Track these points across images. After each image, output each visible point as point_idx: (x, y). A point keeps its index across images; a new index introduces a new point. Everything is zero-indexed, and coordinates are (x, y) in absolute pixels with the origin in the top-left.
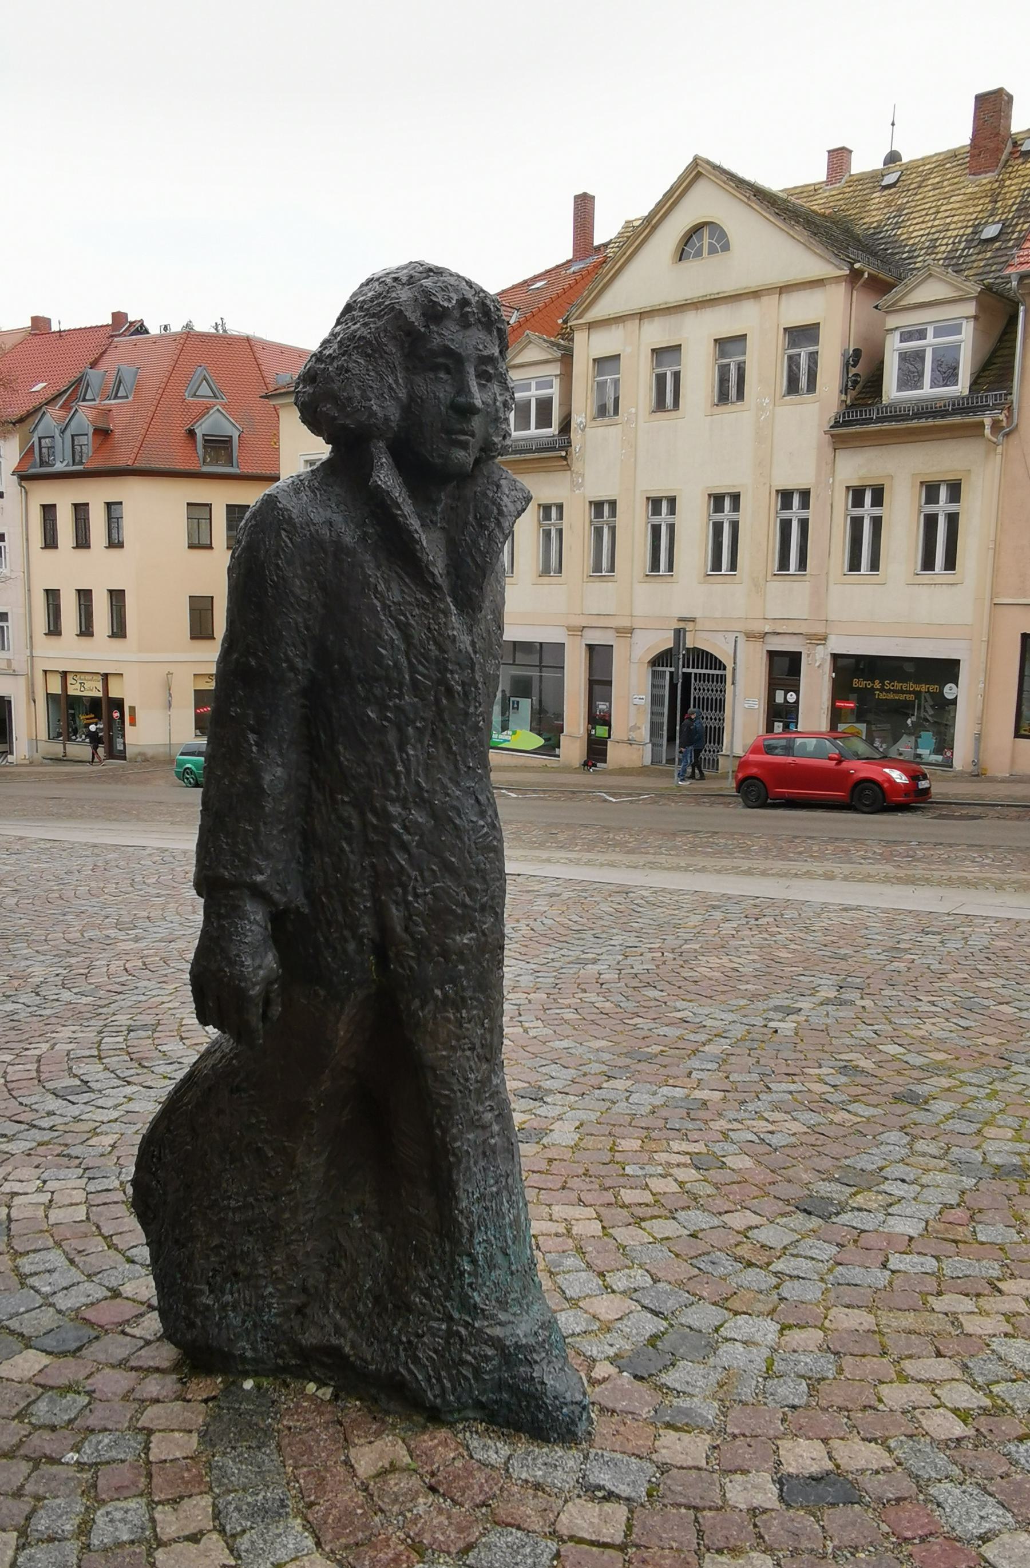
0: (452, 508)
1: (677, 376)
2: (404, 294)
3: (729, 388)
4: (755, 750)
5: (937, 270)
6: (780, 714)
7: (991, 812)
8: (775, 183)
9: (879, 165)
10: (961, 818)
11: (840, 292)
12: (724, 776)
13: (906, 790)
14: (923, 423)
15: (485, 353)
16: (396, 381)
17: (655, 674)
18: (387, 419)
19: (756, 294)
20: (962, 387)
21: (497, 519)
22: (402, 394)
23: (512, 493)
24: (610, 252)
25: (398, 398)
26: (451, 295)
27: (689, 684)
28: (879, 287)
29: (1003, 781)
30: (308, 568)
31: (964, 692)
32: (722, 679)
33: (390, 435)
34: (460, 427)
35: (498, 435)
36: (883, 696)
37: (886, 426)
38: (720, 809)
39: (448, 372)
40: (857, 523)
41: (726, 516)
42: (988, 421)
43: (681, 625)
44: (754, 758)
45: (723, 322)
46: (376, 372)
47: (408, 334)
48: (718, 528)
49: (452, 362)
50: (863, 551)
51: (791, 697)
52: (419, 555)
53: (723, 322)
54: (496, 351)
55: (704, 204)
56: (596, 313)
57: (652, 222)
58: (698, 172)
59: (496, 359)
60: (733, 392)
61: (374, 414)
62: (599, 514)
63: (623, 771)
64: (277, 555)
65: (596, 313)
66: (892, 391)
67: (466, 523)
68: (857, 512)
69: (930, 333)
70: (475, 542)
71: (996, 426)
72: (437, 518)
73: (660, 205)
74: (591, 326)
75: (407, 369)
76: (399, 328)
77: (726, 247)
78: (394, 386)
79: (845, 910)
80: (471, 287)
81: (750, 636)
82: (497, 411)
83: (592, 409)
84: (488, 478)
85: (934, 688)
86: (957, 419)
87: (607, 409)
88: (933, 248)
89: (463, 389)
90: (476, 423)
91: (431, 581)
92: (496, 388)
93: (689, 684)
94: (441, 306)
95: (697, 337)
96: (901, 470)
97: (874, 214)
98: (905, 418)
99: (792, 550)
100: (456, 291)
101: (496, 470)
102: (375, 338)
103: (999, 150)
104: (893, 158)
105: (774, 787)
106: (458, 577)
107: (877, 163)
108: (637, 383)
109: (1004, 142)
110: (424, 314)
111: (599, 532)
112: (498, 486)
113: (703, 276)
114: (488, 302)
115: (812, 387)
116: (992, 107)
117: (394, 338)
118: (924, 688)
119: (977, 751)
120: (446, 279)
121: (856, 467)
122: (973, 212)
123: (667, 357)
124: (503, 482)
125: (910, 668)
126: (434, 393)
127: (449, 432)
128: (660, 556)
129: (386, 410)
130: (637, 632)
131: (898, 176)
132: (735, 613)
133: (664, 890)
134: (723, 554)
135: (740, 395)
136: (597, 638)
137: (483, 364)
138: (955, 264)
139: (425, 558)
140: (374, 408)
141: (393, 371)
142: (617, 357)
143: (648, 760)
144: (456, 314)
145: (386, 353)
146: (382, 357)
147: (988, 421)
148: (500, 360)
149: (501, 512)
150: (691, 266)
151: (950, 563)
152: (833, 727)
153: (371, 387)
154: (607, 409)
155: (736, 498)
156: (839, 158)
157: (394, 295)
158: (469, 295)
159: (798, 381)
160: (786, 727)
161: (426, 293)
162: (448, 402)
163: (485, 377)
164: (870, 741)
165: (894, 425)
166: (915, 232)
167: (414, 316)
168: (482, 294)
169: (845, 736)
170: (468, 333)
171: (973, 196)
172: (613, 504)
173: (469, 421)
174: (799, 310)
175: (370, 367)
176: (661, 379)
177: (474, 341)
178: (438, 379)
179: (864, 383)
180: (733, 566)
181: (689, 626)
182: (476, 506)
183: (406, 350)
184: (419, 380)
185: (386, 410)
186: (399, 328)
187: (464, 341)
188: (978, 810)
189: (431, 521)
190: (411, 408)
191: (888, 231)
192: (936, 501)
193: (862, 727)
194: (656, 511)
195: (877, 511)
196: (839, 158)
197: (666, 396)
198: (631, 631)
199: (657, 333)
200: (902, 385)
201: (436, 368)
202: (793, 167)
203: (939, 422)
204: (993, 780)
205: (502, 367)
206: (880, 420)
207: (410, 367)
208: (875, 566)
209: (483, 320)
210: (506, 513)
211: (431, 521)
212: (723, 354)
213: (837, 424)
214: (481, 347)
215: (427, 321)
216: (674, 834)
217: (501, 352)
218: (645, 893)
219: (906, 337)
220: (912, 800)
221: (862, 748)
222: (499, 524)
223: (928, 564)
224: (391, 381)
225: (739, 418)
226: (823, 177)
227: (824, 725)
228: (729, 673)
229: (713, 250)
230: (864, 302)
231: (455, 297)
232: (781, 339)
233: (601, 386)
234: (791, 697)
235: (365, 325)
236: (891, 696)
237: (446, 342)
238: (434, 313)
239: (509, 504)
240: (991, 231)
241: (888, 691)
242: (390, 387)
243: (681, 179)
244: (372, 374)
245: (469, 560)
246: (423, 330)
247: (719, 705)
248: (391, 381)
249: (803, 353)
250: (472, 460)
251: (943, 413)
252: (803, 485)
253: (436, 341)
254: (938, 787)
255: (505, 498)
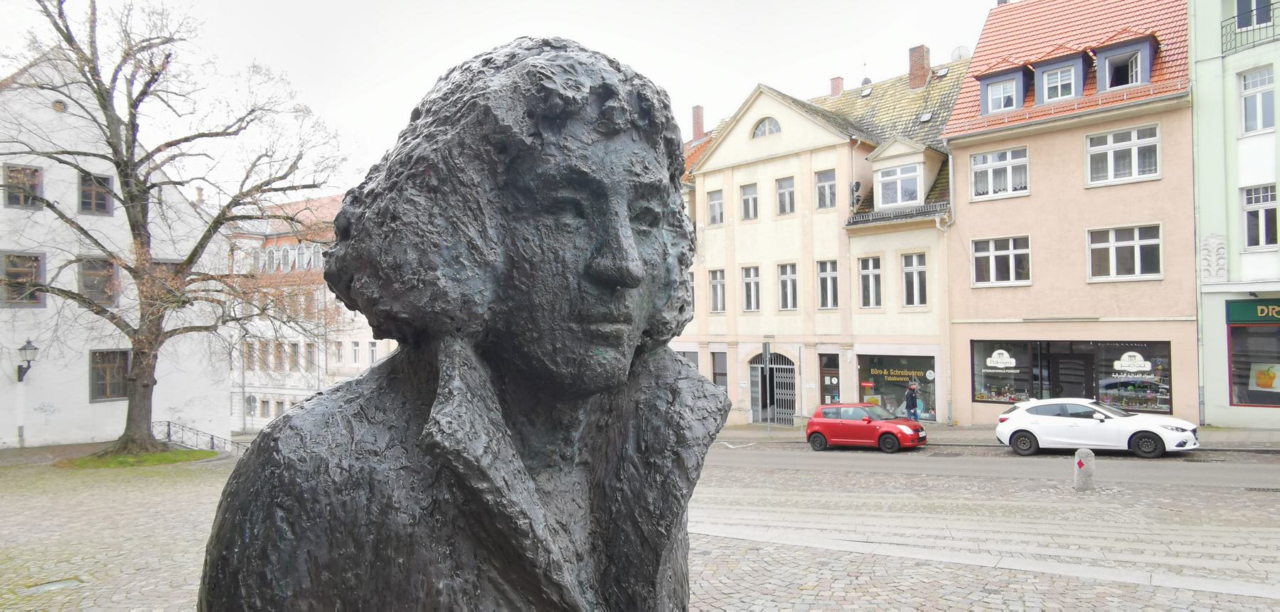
0: (599, 428)
1: (755, 200)
2: (497, 82)
3: (785, 206)
4: (817, 415)
5: (899, 138)
6: (829, 391)
7: (966, 450)
8: (803, 97)
9: (860, 86)
10: (949, 455)
11: (845, 151)
12: (798, 429)
13: (912, 438)
14: (899, 221)
15: (646, 179)
16: (483, 233)
17: (752, 369)
18: (466, 302)
19: (797, 154)
20: (920, 201)
21: (676, 453)
22: (496, 256)
23: (700, 403)
24: (713, 135)
25: (487, 264)
26: (582, 79)
27: (773, 379)
28: (868, 148)
29: (969, 429)
30: (325, 575)
31: (938, 375)
32: (792, 371)
33: (475, 327)
34: (603, 310)
35: (671, 308)
36: (890, 379)
37: (878, 223)
38: (798, 452)
39: (579, 212)
40: (865, 279)
41: (789, 276)
42: (937, 220)
43: (766, 340)
44: (816, 420)
45: (781, 170)
46: (447, 219)
47: (502, 148)
48: (784, 284)
49: (586, 195)
50: (870, 294)
51: (835, 381)
52: (529, 555)
53: (781, 170)
54: (665, 176)
55: (765, 107)
56: (707, 168)
57: (736, 119)
58: (759, 92)
59: (666, 189)
60: (788, 208)
61: (441, 295)
62: (714, 277)
63: (736, 427)
64: (264, 556)
65: (707, 168)
66: (879, 204)
67: (622, 458)
68: (865, 272)
69: (899, 171)
70: (639, 496)
71: (943, 222)
72: (573, 451)
73: (741, 109)
74: (705, 174)
75: (504, 211)
76: (485, 138)
77: (779, 130)
78: (479, 242)
79: (918, 564)
80: (619, 70)
81: (807, 345)
82: (668, 271)
83: (708, 219)
84: (658, 377)
85: (920, 374)
86: (920, 219)
87: (717, 219)
88: (894, 127)
89: (606, 242)
90: (634, 301)
91: (555, 598)
92: (664, 234)
93: (773, 379)
94: (561, 96)
95: (765, 179)
96: (890, 247)
97: (858, 111)
98: (889, 219)
99: (829, 294)
100: (590, 72)
101: (669, 363)
102: (444, 158)
103: (925, 76)
104: (867, 81)
105: (828, 438)
106: (610, 559)
107: (858, 84)
108: (732, 205)
109: (927, 71)
110: (530, 114)
111: (715, 288)
112: (675, 392)
113: (766, 146)
114: (649, 94)
115: (833, 203)
116: (918, 55)
117: (477, 157)
118: (913, 373)
119: (950, 411)
120: (571, 54)
121: (864, 246)
122: (914, 108)
123: (749, 190)
124: (682, 384)
125: (904, 362)
126: (556, 253)
127: (583, 319)
128: (751, 299)
129: (467, 285)
130: (740, 346)
131: (868, 91)
132: (799, 333)
133: (783, 546)
134: (788, 298)
135: (792, 209)
136: (717, 349)
137: (643, 197)
138: (908, 134)
139: (542, 559)
140: (442, 282)
141: (477, 214)
142: (721, 191)
143: (751, 420)
144: (591, 112)
145: (462, 183)
146: (455, 191)
147: (937, 220)
148: (672, 190)
149: (681, 440)
150: (760, 141)
151: (923, 300)
152: (861, 400)
153: (436, 245)
154: (717, 219)
155: (793, 266)
156: (837, 82)
157: (480, 84)
158: (614, 79)
159: (825, 200)
160: (833, 398)
161: (535, 76)
162: (581, 267)
163: (646, 219)
164: (884, 405)
165: (883, 223)
166: (883, 119)
167: (512, 118)
168: (636, 81)
169: (871, 404)
170: (616, 144)
171: (913, 100)
172: (722, 271)
173: (621, 298)
174: (824, 162)
175: (436, 210)
176: (746, 202)
177: (622, 160)
178: (561, 228)
179: (864, 202)
180: (795, 305)
181: (770, 340)
182: (638, 427)
183: (502, 179)
184: (525, 230)
185: (467, 285)
186: (485, 138)
187: (607, 160)
188: (957, 450)
189: (563, 458)
190: (513, 279)
191: (868, 119)
192: (911, 265)
193: (879, 397)
194: (748, 275)
195: (877, 272)
196: (837, 82)
197: (750, 210)
198: (736, 344)
199: (742, 177)
200: (885, 201)
201: (556, 208)
202: (815, 90)
203: (909, 220)
204: (962, 429)
205: (674, 201)
206: (874, 220)
207: (510, 207)
208: (878, 302)
209: (641, 123)
210: (692, 442)
211: (563, 458)
212: (780, 187)
213: (849, 224)
214: (638, 169)
215: (536, 125)
216: (772, 472)
217: (672, 178)
218: (771, 549)
219: (886, 174)
220: (914, 444)
221: (879, 410)
222: (678, 460)
223: (910, 300)
224: (473, 233)
225: (791, 222)
226: (829, 93)
227: (856, 399)
228: (796, 367)
229: (771, 132)
230: (859, 157)
231: (587, 83)
232: (814, 178)
233: (712, 207)
234: (835, 381)
235: (430, 137)
236: (894, 379)
237: (574, 162)
238: (550, 111)
239: (696, 424)
240: (926, 117)
241: (893, 375)
242: (472, 246)
243: (752, 95)
244: (439, 221)
245: (628, 527)
246: (529, 141)
247: (791, 386)
248: (473, 233)
249: (827, 185)
250: (627, 362)
251: (911, 215)
252: (833, 259)
253: (554, 162)
254: (929, 434)
255: (688, 415)
